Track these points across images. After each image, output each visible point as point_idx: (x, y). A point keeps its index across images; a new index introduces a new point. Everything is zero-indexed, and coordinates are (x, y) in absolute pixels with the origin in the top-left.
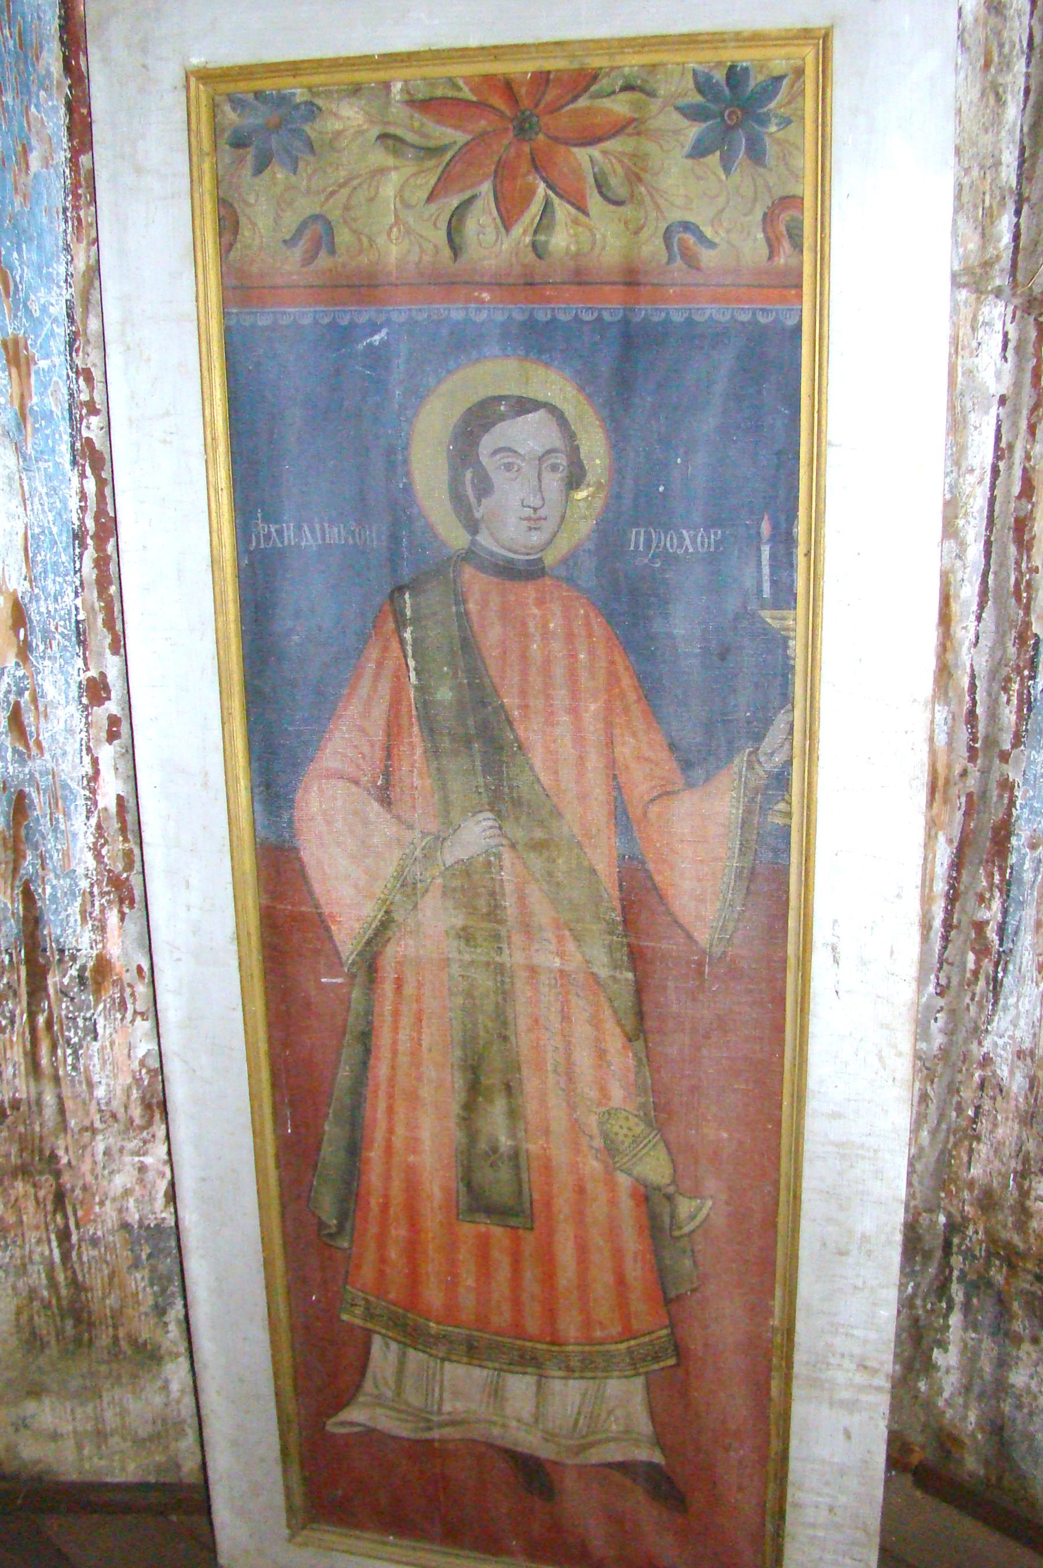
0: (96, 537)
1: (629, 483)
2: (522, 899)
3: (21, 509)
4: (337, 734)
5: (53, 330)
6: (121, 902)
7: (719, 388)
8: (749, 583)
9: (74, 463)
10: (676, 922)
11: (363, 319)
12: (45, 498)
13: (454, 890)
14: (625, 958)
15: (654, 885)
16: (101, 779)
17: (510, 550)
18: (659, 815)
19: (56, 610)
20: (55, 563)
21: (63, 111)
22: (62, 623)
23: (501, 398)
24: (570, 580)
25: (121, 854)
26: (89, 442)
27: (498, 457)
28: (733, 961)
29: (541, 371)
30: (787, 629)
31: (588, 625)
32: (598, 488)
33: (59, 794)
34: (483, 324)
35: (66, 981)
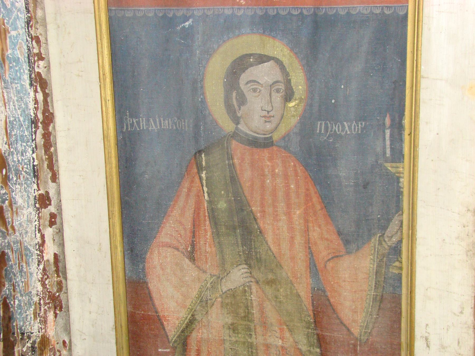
0: (43, 123)
1: (317, 98)
2: (262, 311)
3: (3, 108)
4: (168, 225)
5: (18, 15)
6: (55, 308)
7: (364, 48)
8: (379, 149)
9: (31, 85)
10: (342, 323)
11: (180, 14)
12: (16, 102)
13: (227, 304)
14: (315, 341)
15: (330, 303)
16: (46, 245)
17: (255, 132)
18: (332, 268)
19: (22, 159)
20: (22, 136)
22: (26, 166)
23: (251, 55)
24: (286, 148)
25: (55, 283)
26: (39, 74)
27: (249, 85)
28: (372, 344)
29: (271, 40)
30: (399, 173)
31: (295, 171)
32: (300, 102)
33: (23, 253)
34: (241, 16)
35: (25, 349)
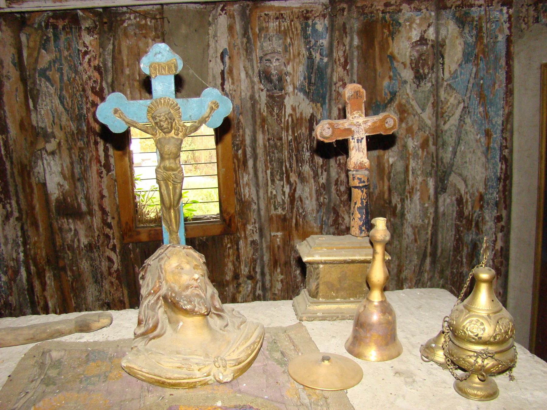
9: (500, 161)
21: (505, 74)
